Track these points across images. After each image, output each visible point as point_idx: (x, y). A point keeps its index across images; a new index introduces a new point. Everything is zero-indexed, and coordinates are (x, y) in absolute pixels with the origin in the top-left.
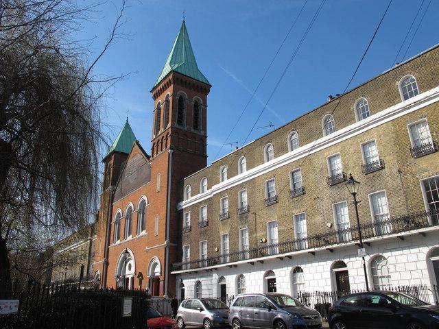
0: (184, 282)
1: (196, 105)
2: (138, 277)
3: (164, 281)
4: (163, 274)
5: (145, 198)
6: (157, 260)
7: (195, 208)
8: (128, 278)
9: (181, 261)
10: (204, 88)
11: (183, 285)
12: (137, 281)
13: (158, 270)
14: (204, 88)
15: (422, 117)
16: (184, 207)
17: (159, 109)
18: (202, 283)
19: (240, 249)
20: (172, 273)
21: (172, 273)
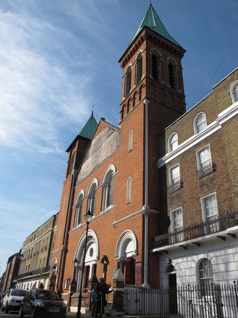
0: (174, 262)
1: (171, 67)
2: (102, 262)
3: (143, 262)
4: (140, 252)
5: (112, 167)
6: (131, 235)
7: (188, 158)
8: (88, 267)
9: (167, 232)
10: (179, 52)
11: (171, 268)
12: (100, 267)
13: (131, 249)
14: (179, 52)
15: (179, 206)
16: (166, 162)
17: (129, 74)
18: (213, 261)
19: (204, 220)
20: (154, 250)
21: (154, 250)
